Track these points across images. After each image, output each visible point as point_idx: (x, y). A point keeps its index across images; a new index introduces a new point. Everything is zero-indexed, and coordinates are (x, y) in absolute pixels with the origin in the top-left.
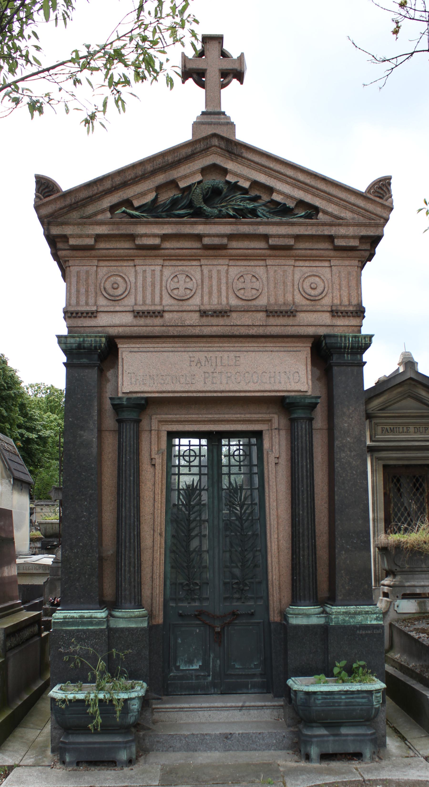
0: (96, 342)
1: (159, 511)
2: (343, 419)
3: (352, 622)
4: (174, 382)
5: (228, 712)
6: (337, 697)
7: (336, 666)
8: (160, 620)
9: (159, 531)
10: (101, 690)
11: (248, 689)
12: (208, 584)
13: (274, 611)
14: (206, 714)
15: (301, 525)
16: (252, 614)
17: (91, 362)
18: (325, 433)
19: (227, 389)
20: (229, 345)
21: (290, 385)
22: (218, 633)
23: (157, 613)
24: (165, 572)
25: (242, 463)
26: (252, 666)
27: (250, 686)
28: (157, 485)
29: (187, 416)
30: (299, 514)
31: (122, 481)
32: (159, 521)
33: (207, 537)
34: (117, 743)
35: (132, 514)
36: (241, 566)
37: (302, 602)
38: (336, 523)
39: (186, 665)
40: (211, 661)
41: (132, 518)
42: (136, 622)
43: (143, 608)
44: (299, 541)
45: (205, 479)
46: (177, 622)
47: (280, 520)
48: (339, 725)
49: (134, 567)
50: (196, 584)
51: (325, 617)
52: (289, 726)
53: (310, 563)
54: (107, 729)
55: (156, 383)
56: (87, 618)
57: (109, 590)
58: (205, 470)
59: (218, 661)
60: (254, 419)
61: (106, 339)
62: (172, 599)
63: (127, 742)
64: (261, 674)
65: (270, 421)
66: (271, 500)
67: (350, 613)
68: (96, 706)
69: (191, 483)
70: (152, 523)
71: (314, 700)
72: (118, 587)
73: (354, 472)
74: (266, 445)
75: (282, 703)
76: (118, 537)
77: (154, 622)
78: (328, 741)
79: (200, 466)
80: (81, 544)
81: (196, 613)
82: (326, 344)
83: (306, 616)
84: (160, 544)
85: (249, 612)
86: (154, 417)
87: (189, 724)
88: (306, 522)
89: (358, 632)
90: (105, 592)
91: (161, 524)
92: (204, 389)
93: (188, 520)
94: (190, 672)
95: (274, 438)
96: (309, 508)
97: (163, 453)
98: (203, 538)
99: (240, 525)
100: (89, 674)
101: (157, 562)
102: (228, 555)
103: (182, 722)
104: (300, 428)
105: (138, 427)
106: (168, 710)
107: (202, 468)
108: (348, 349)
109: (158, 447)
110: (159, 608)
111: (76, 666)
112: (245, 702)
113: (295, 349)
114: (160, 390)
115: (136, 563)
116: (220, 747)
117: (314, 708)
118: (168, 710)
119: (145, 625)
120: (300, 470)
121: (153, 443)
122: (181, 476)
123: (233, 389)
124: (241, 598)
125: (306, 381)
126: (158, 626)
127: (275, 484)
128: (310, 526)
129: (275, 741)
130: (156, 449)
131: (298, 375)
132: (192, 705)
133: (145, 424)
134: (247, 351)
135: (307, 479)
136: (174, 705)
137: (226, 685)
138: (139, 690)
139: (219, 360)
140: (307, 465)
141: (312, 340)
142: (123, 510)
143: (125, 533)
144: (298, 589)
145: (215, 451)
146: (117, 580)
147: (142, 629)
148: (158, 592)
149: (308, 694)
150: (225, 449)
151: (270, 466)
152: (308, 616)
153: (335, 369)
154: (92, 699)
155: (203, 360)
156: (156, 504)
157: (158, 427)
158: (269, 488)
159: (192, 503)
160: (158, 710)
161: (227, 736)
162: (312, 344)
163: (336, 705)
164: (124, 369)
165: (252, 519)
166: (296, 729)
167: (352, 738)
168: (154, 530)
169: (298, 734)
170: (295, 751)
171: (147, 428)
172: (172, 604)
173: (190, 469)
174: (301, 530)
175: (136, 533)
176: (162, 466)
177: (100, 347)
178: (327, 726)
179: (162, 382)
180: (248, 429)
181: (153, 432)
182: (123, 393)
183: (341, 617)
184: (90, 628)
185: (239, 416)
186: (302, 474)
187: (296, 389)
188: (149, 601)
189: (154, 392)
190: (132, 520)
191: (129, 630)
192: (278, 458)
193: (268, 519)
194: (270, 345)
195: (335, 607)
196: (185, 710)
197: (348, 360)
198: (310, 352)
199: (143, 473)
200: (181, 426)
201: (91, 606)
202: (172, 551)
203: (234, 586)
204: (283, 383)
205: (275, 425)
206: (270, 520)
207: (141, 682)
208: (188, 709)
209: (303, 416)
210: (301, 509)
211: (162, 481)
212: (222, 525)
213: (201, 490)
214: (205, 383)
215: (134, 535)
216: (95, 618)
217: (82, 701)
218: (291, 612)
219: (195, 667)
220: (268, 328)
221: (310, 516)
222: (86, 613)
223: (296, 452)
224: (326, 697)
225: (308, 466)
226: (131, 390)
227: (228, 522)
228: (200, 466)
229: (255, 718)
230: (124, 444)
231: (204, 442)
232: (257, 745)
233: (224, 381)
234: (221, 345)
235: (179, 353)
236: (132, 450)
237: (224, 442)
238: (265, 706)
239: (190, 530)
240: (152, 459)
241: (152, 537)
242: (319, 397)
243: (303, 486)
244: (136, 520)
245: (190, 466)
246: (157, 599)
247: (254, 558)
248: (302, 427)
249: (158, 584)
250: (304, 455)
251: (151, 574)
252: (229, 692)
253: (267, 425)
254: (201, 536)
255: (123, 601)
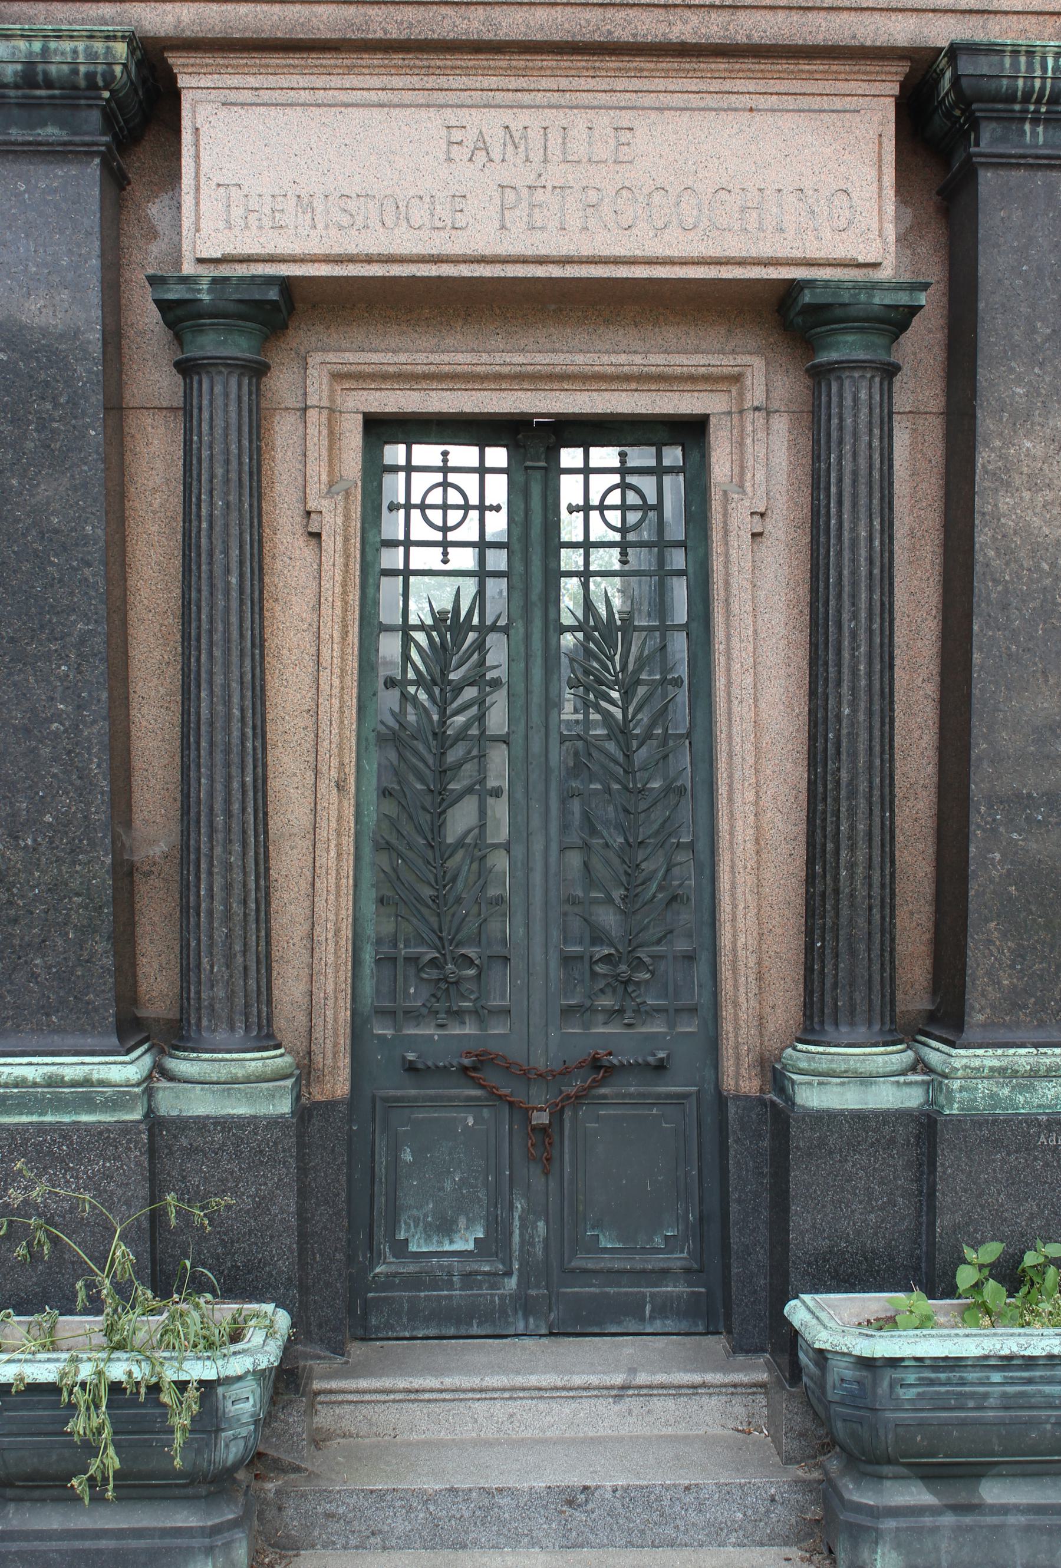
0: (91, 55)
1: (336, 702)
2: (1011, 370)
3: (1025, 1102)
4: (389, 223)
5: (574, 1405)
6: (972, 1376)
7: (964, 1261)
8: (338, 1084)
9: (334, 774)
10: (120, 1346)
11: (642, 1319)
12: (506, 959)
13: (738, 1058)
14: (500, 1409)
15: (844, 757)
16: (660, 1067)
17: (77, 139)
18: (933, 430)
19: (586, 251)
20: (591, 83)
21: (819, 239)
22: (543, 1130)
23: (329, 1062)
24: (355, 920)
25: (631, 537)
26: (658, 1241)
27: (648, 1308)
28: (326, 610)
29: (435, 358)
30: (838, 718)
31: (199, 591)
32: (335, 739)
33: (505, 796)
34: (177, 1532)
35: (236, 712)
36: (624, 899)
37: (844, 1029)
38: (975, 753)
39: (428, 1239)
40: (517, 1223)
41: (236, 726)
42: (250, 1097)
43: (277, 1047)
44: (837, 813)
45: (496, 588)
46: (399, 1093)
47: (766, 739)
48: (976, 1473)
49: (245, 902)
50: (469, 962)
51: (923, 1082)
52: (789, 1461)
53: (876, 891)
54: (138, 1484)
55: (320, 226)
56: (74, 1084)
57: (157, 983)
58: (497, 560)
59: (541, 1224)
60: (679, 370)
61: (132, 50)
62: (381, 1012)
63: (215, 1531)
64: (688, 1271)
65: (736, 379)
66: (736, 667)
67: (1015, 1074)
68: (97, 1407)
69: (450, 607)
70: (309, 745)
71: (891, 1387)
72: (188, 970)
73: (1046, 567)
74: (721, 466)
75: (763, 1377)
76: (186, 795)
77: (319, 1094)
78: (935, 1530)
79: (482, 545)
80: (48, 818)
81: (466, 1062)
82: (956, 79)
83: (856, 1080)
84: (339, 819)
85: (651, 1059)
86: (315, 359)
87: (441, 1444)
88: (862, 747)
89: (1043, 1139)
90: (143, 987)
91: (341, 748)
92: (501, 250)
93: (439, 735)
94: (445, 1261)
95: (749, 441)
96: (877, 698)
97: (347, 494)
98: (490, 801)
99: (621, 758)
100: (79, 1284)
101: (326, 883)
102: (575, 859)
103: (415, 1437)
104: (848, 402)
105: (257, 393)
106: (367, 1397)
107: (490, 553)
108: (1039, 101)
109: (331, 473)
110: (336, 1045)
111: (35, 1256)
112: (633, 1371)
113: (838, 103)
114: (337, 250)
115: (252, 885)
116: (547, 1535)
117: (888, 1414)
118: (367, 1397)
119: (284, 1107)
120: (846, 555)
121: (312, 454)
122: (413, 550)
123: (605, 252)
124: (621, 1011)
125: (875, 226)
126: (330, 1105)
127: (749, 608)
128: (878, 762)
129: (739, 1515)
130: (324, 477)
131: (846, 204)
132: (449, 1381)
133: (281, 383)
134: (660, 109)
135: (871, 590)
136: (387, 1383)
137: (570, 1307)
138: (264, 1335)
139: (555, 139)
140: (871, 539)
141: (902, 68)
142: (203, 694)
143: (212, 779)
144: (829, 982)
145: (536, 490)
146: (185, 946)
147: (274, 1122)
148: (330, 988)
149: (867, 1363)
150: (570, 490)
151: (734, 542)
152: (865, 1079)
153: (988, 180)
154: (83, 1385)
155: (496, 138)
156: (324, 675)
157: (332, 400)
158: (728, 625)
159: (452, 676)
160: (333, 1398)
161: (573, 1499)
162: (902, 86)
163: (971, 1404)
164: (203, 170)
165: (666, 735)
166: (816, 1475)
167: (1023, 1519)
168: (316, 771)
169: (826, 1493)
170: (813, 1551)
171: (292, 401)
172: (383, 1030)
173: (445, 554)
174: (844, 776)
175: (249, 779)
176: (346, 540)
177: (109, 78)
178: (931, 1474)
179: (346, 220)
180: (657, 411)
181: (313, 414)
182: (201, 261)
183: (983, 1087)
184: (85, 1118)
185: (623, 358)
186: (854, 573)
187: (840, 253)
188: (301, 1018)
189: (314, 259)
190: (236, 734)
191: (224, 1123)
192: (762, 515)
193: (722, 737)
194: (744, 83)
195: (962, 1052)
196: (427, 1396)
197: (1037, 146)
198: (892, 116)
199: (279, 565)
200: (415, 395)
201: (90, 1042)
202: (383, 846)
203: (600, 969)
204: (790, 233)
205: (756, 395)
206: (730, 737)
207: (269, 1308)
208: (435, 1396)
209: (861, 355)
210: (846, 696)
211: (345, 593)
212: (557, 755)
213: (484, 630)
214: (503, 227)
215: (243, 784)
216: (102, 1083)
217: (52, 1389)
218: (803, 1065)
219: (459, 1246)
220: (742, 16)
221: (877, 725)
222: (71, 1068)
223: (833, 490)
224: (933, 1375)
225: (877, 543)
226: (229, 250)
227: (580, 744)
228: (482, 545)
229: (667, 1424)
230: (205, 454)
231: (497, 456)
232: (677, 1527)
233: (574, 222)
234: (564, 83)
235: (409, 111)
236: (233, 476)
237: (570, 457)
238: (704, 1385)
239: (444, 773)
240: (309, 513)
241: (308, 792)
242: (925, 287)
243: (855, 616)
244: (249, 731)
245: (445, 545)
246: (329, 1013)
247: (668, 870)
248: (856, 399)
249: (331, 959)
250: (863, 501)
251: (307, 927)
252: (578, 1330)
253: (724, 397)
254: (482, 791)
255: (205, 1022)
